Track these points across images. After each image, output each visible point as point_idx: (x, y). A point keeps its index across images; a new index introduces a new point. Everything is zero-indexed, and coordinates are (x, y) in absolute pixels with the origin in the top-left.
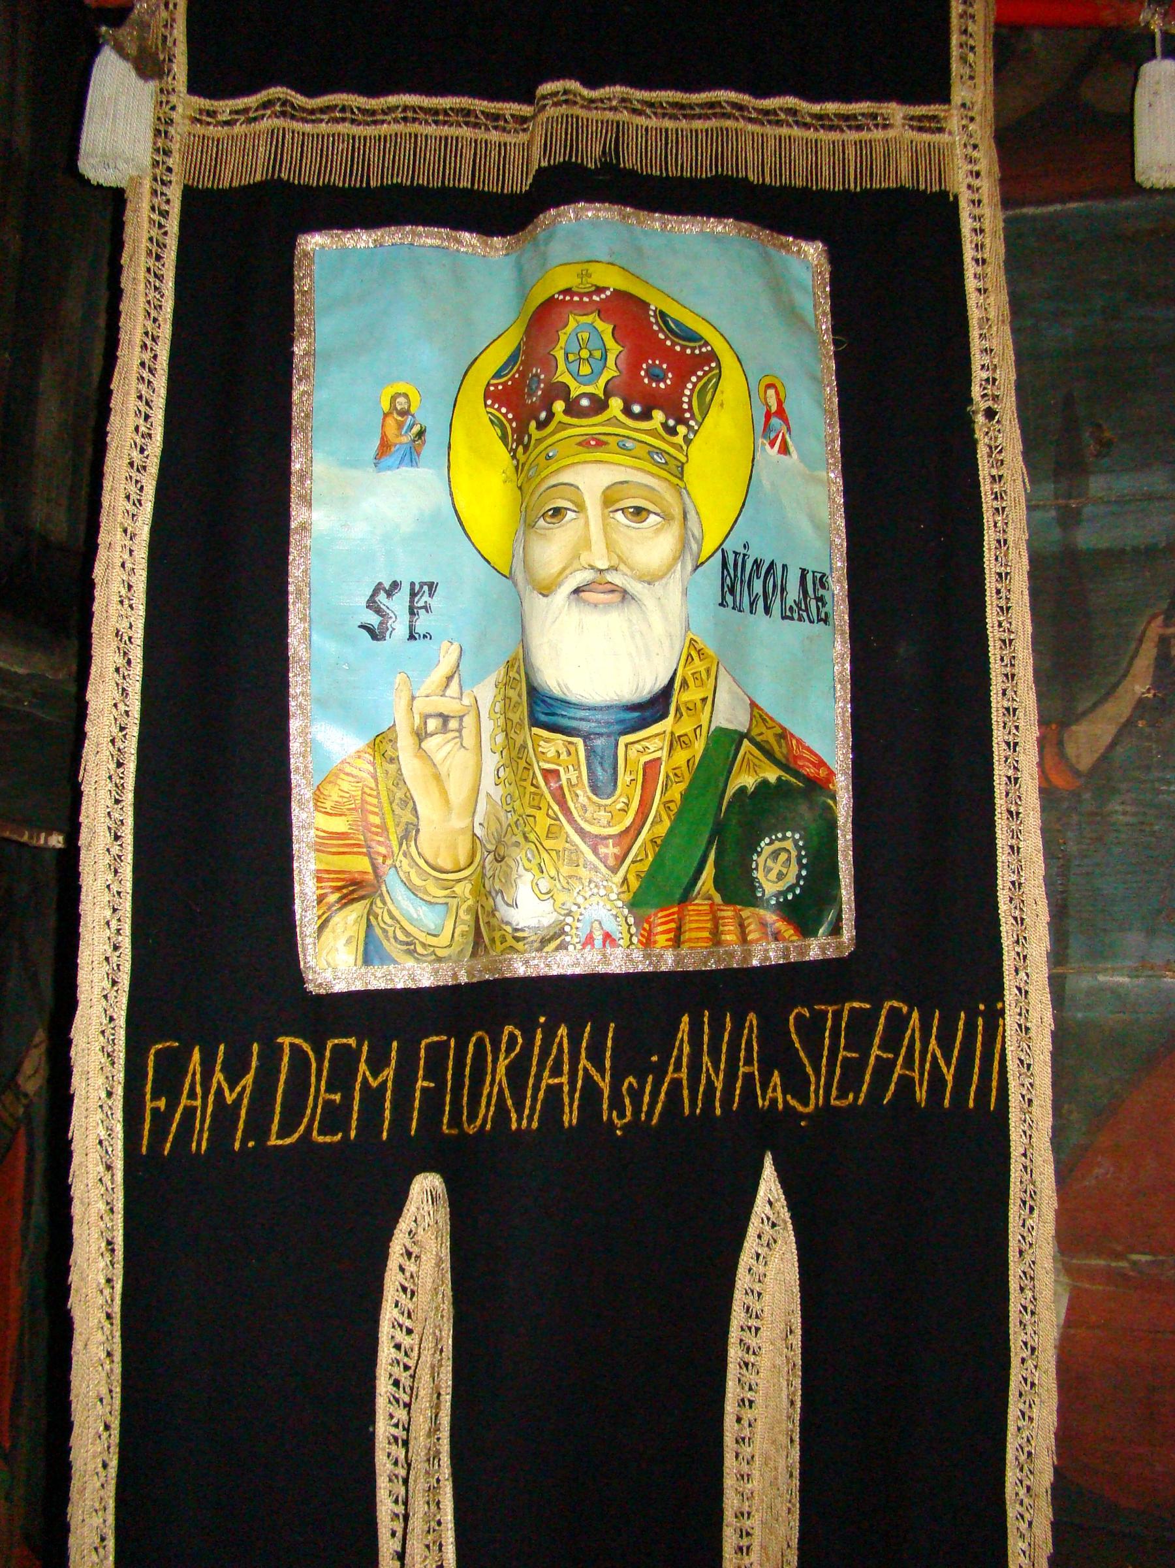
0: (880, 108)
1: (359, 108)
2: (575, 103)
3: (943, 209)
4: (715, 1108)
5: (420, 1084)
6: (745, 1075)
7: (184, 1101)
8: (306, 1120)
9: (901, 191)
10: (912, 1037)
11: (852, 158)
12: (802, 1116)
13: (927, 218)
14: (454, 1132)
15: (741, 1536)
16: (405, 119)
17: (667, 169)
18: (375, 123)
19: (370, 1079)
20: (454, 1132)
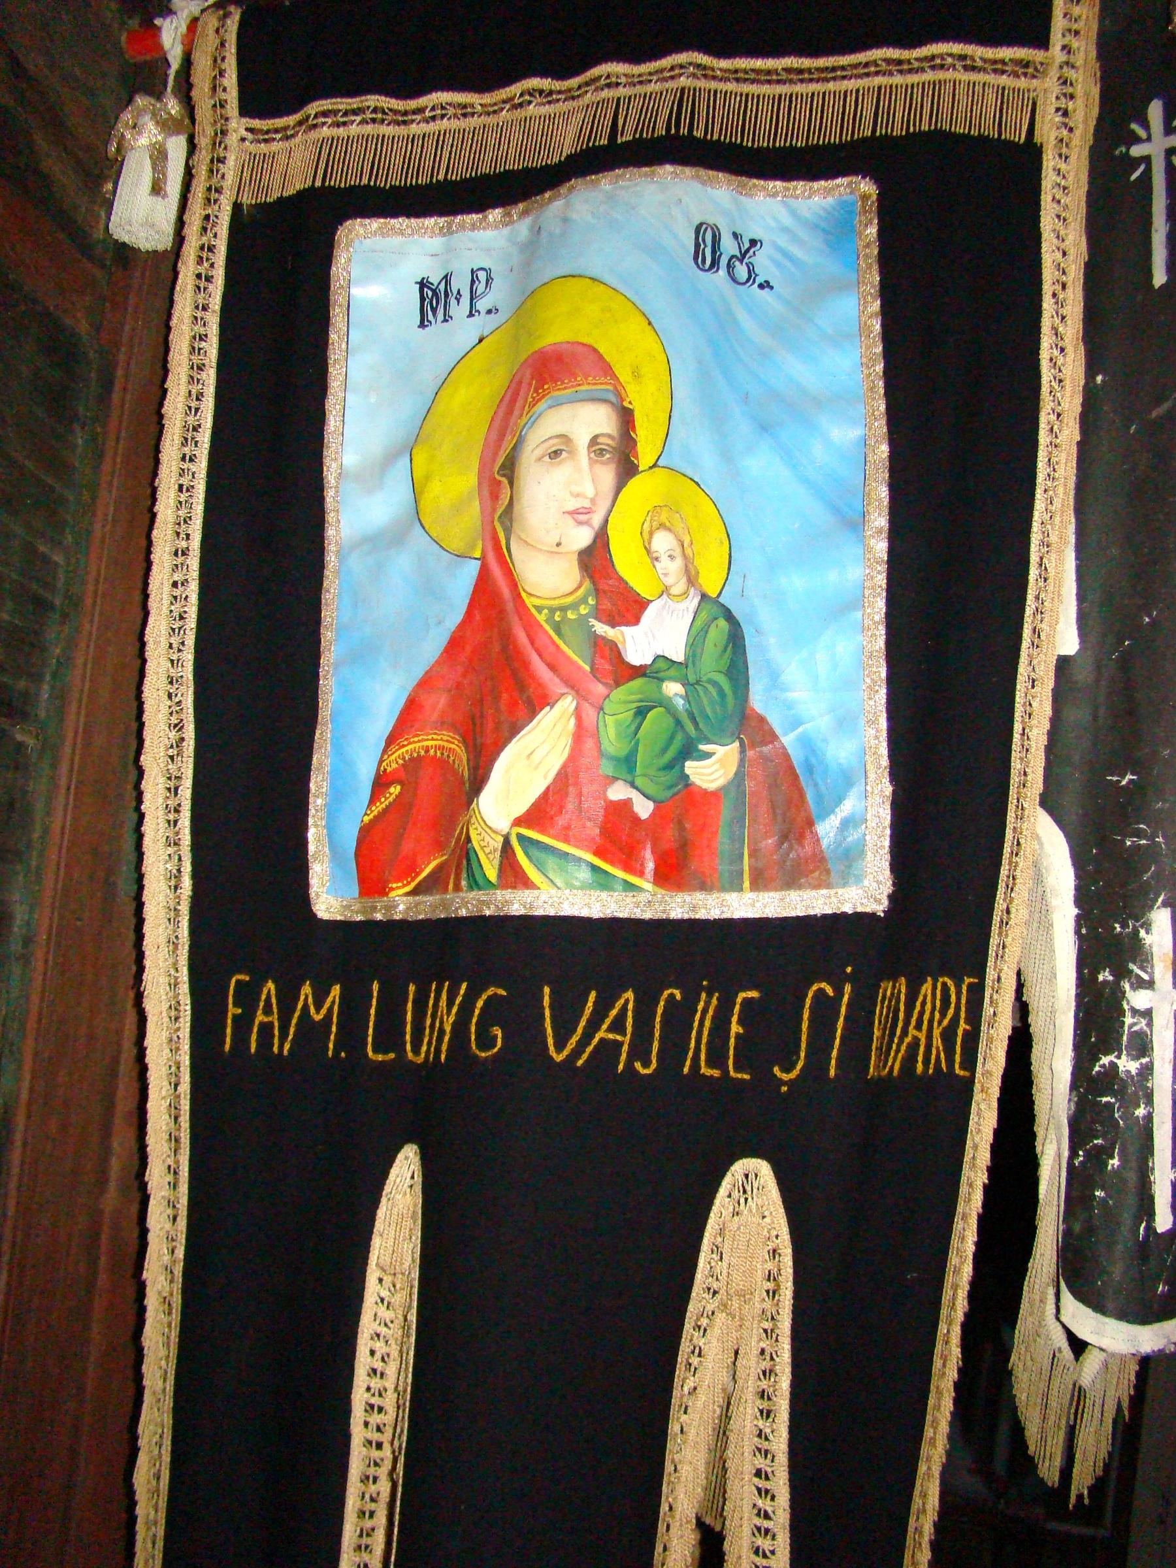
0: (362, 102)
1: (391, 110)
2: (618, 84)
3: (1028, 156)
4: (684, 1065)
5: (276, 1016)
6: (262, 1024)
7: (260, 1017)
8: (690, 1054)
9: (983, 139)
10: (333, 1002)
11: (899, 115)
12: (782, 1082)
13: (1013, 168)
14: (716, 1073)
15: (369, 1466)
16: (374, 121)
17: (914, 125)
18: (405, 123)
19: (312, 1010)
20: (716, 1073)
